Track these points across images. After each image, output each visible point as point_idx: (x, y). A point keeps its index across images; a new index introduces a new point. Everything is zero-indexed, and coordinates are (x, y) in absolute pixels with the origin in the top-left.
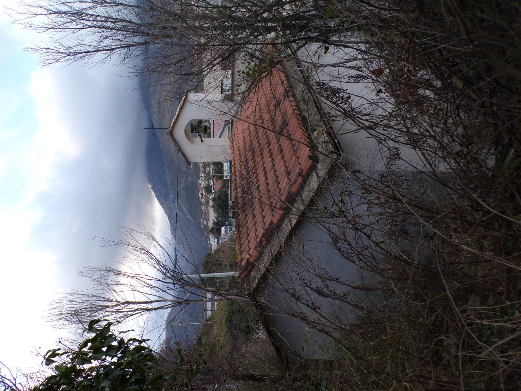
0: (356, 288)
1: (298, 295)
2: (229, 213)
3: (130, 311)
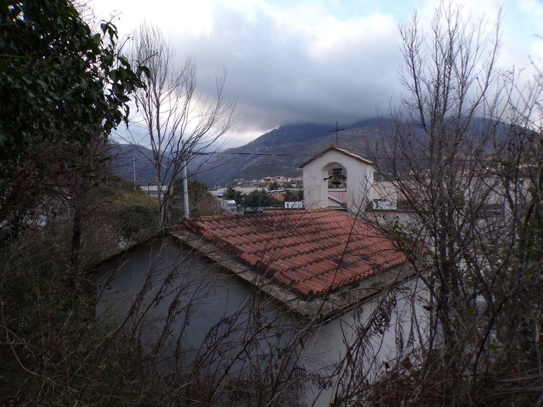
0: (178, 345)
1: (171, 281)
2: (250, 208)
3: (149, 107)
